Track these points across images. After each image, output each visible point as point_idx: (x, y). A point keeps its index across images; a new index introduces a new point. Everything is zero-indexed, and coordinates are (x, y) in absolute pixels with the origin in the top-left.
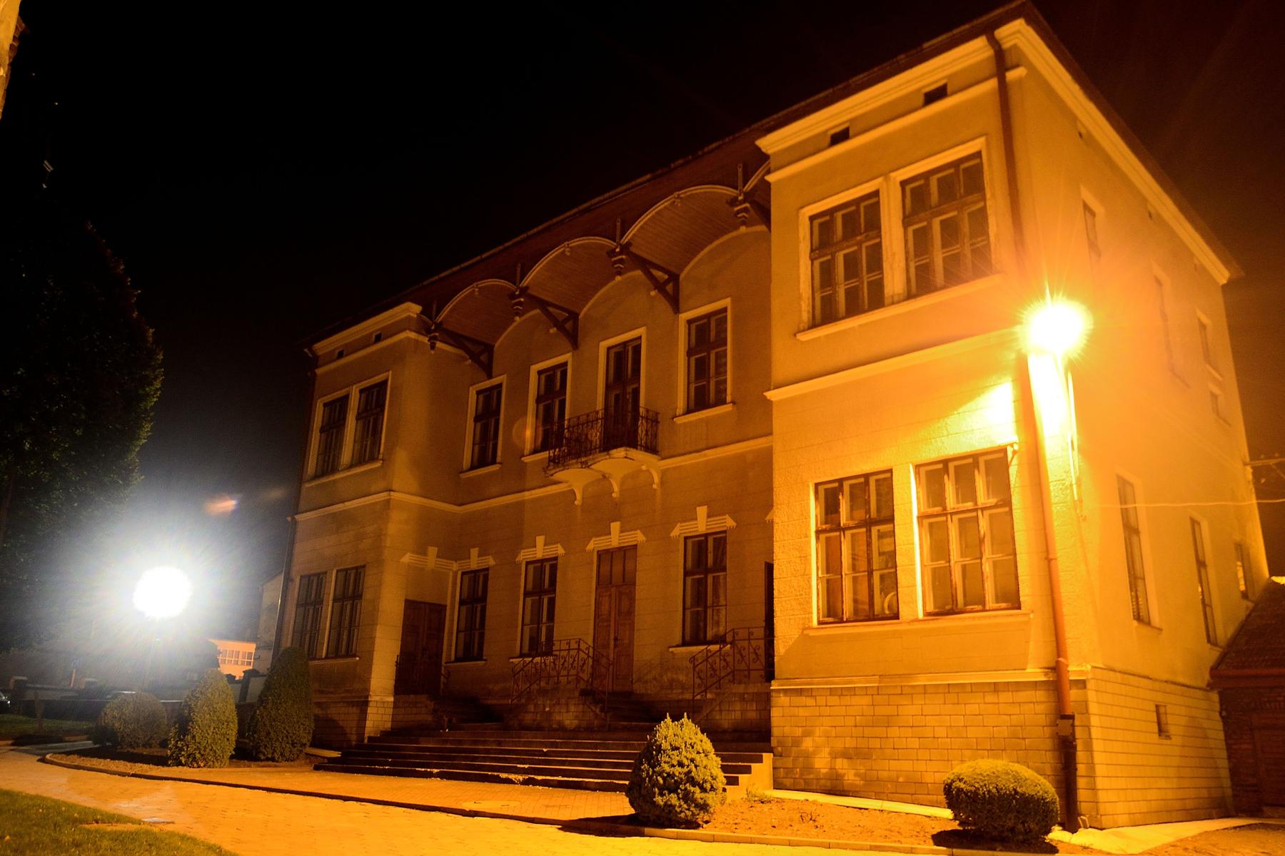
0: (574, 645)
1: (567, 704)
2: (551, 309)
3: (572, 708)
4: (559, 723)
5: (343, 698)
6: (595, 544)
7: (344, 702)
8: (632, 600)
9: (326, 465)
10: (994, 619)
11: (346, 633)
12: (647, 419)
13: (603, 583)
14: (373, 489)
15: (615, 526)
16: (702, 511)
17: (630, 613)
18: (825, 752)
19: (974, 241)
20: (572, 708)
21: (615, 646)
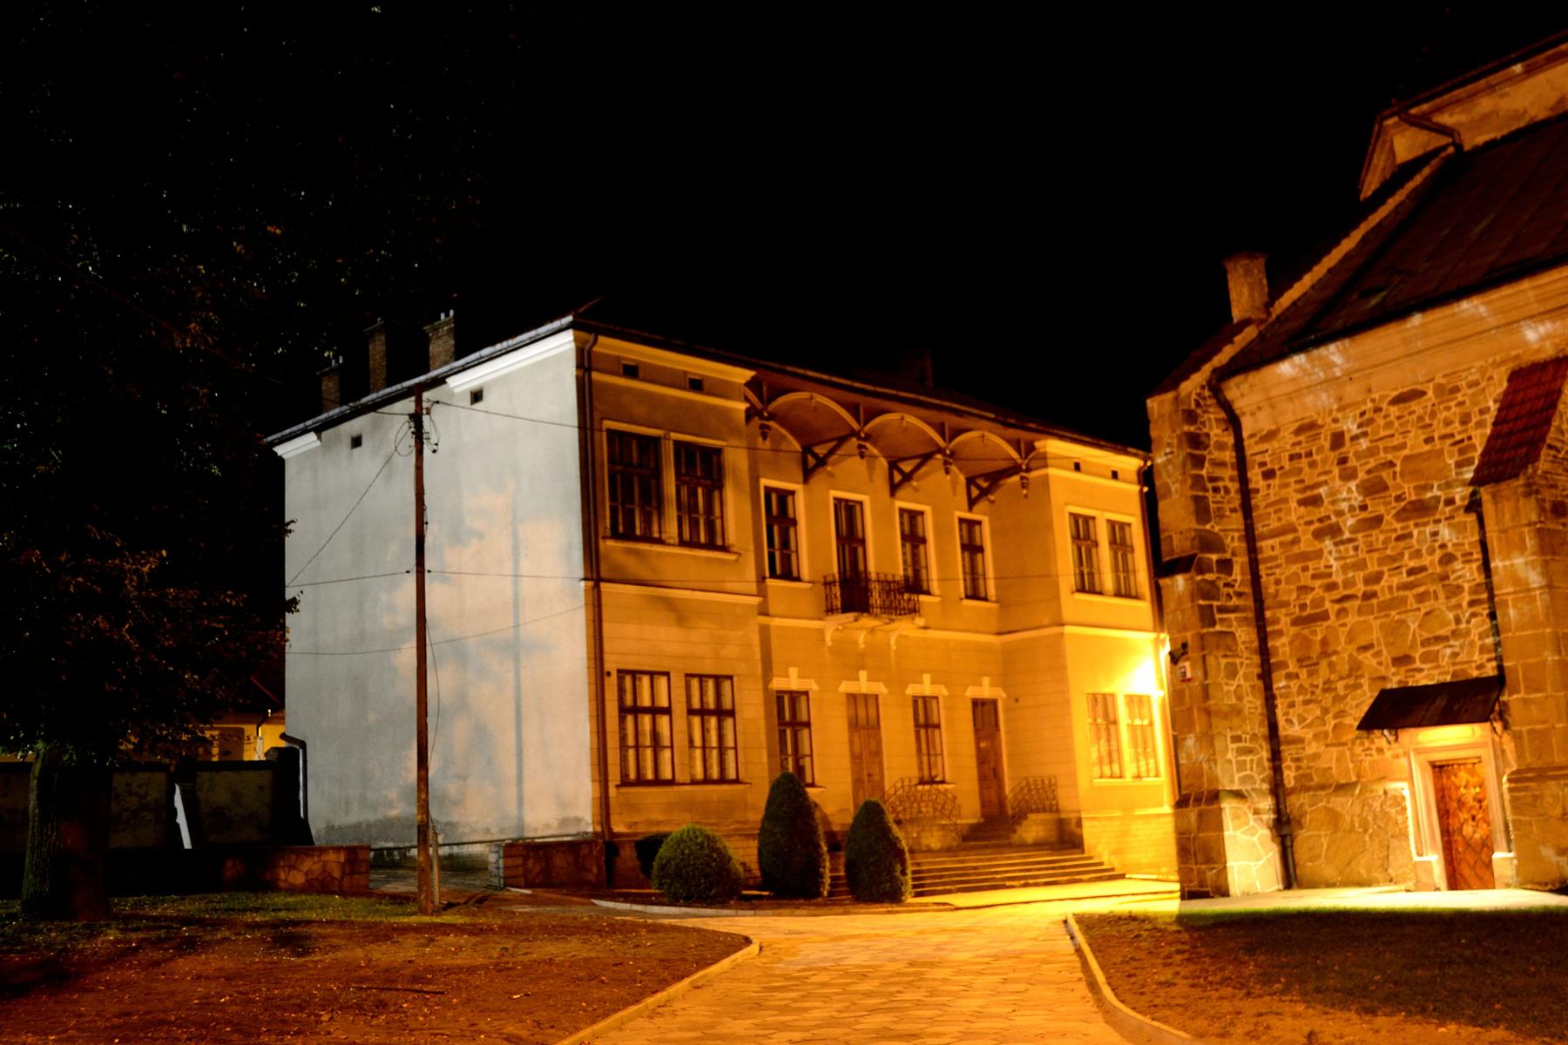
0: (906, 783)
1: (931, 830)
2: (834, 443)
3: (935, 833)
4: (928, 846)
5: (736, 830)
6: (846, 687)
7: (741, 835)
8: (879, 743)
9: (1530, 775)
10: (1150, 780)
11: (715, 753)
12: (878, 581)
13: (854, 725)
14: (729, 586)
15: (863, 674)
16: (927, 678)
17: (878, 753)
18: (1106, 852)
19: (1526, 739)
20: (935, 833)
21: (869, 780)
